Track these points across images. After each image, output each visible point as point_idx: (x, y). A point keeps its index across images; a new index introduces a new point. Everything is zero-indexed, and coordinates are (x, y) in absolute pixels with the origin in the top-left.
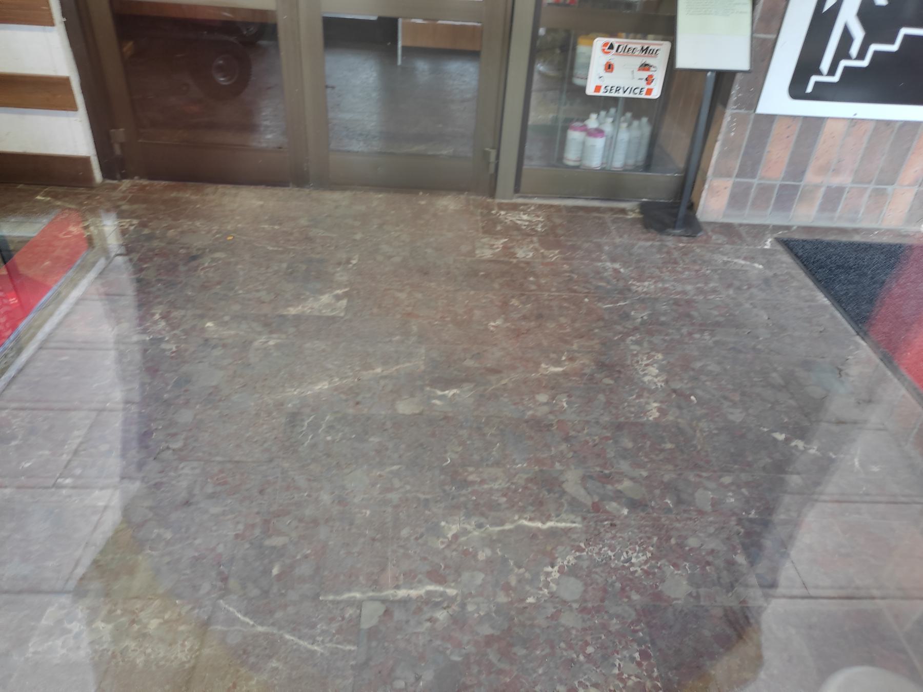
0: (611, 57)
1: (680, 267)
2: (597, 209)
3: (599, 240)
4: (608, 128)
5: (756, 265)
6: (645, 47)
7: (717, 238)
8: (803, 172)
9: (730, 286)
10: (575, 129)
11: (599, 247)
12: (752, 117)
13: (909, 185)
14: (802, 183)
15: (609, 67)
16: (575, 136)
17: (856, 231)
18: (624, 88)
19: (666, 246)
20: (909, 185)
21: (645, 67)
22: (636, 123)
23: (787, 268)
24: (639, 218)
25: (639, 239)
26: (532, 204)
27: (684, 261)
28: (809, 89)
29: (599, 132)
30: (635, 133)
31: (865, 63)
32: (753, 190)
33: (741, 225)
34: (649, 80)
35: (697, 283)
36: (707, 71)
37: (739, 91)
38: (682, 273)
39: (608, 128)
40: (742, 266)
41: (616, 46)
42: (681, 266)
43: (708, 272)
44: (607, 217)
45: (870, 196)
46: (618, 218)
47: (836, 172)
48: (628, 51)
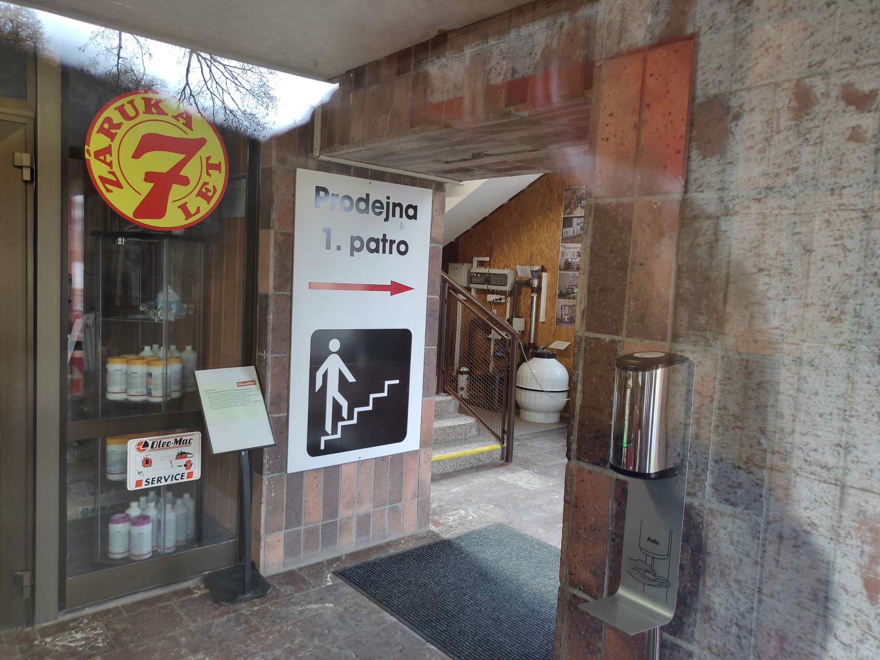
0: (148, 453)
1: (262, 633)
2: (160, 598)
3: (172, 634)
4: (152, 512)
5: (327, 605)
6: (178, 440)
7: (283, 589)
8: (336, 510)
9: (313, 636)
10: (117, 522)
11: (175, 641)
12: (285, 477)
13: (411, 499)
14: (338, 519)
15: (147, 462)
16: (118, 529)
17: (389, 544)
18: (165, 477)
19: (242, 614)
20: (411, 499)
21: (182, 455)
22: (179, 501)
23: (352, 598)
24: (205, 594)
25: (214, 617)
26: (84, 617)
27: (264, 625)
28: (322, 447)
29: (143, 519)
30: (181, 510)
31: (354, 421)
32: (302, 536)
33: (300, 569)
34: (188, 465)
35: (284, 644)
36: (239, 452)
37: (270, 460)
38: (267, 639)
39: (152, 512)
40: (316, 611)
41: (150, 443)
42: (263, 631)
43: (290, 628)
44: (173, 603)
45: (389, 514)
46: (183, 601)
47: (360, 503)
48: (162, 446)
